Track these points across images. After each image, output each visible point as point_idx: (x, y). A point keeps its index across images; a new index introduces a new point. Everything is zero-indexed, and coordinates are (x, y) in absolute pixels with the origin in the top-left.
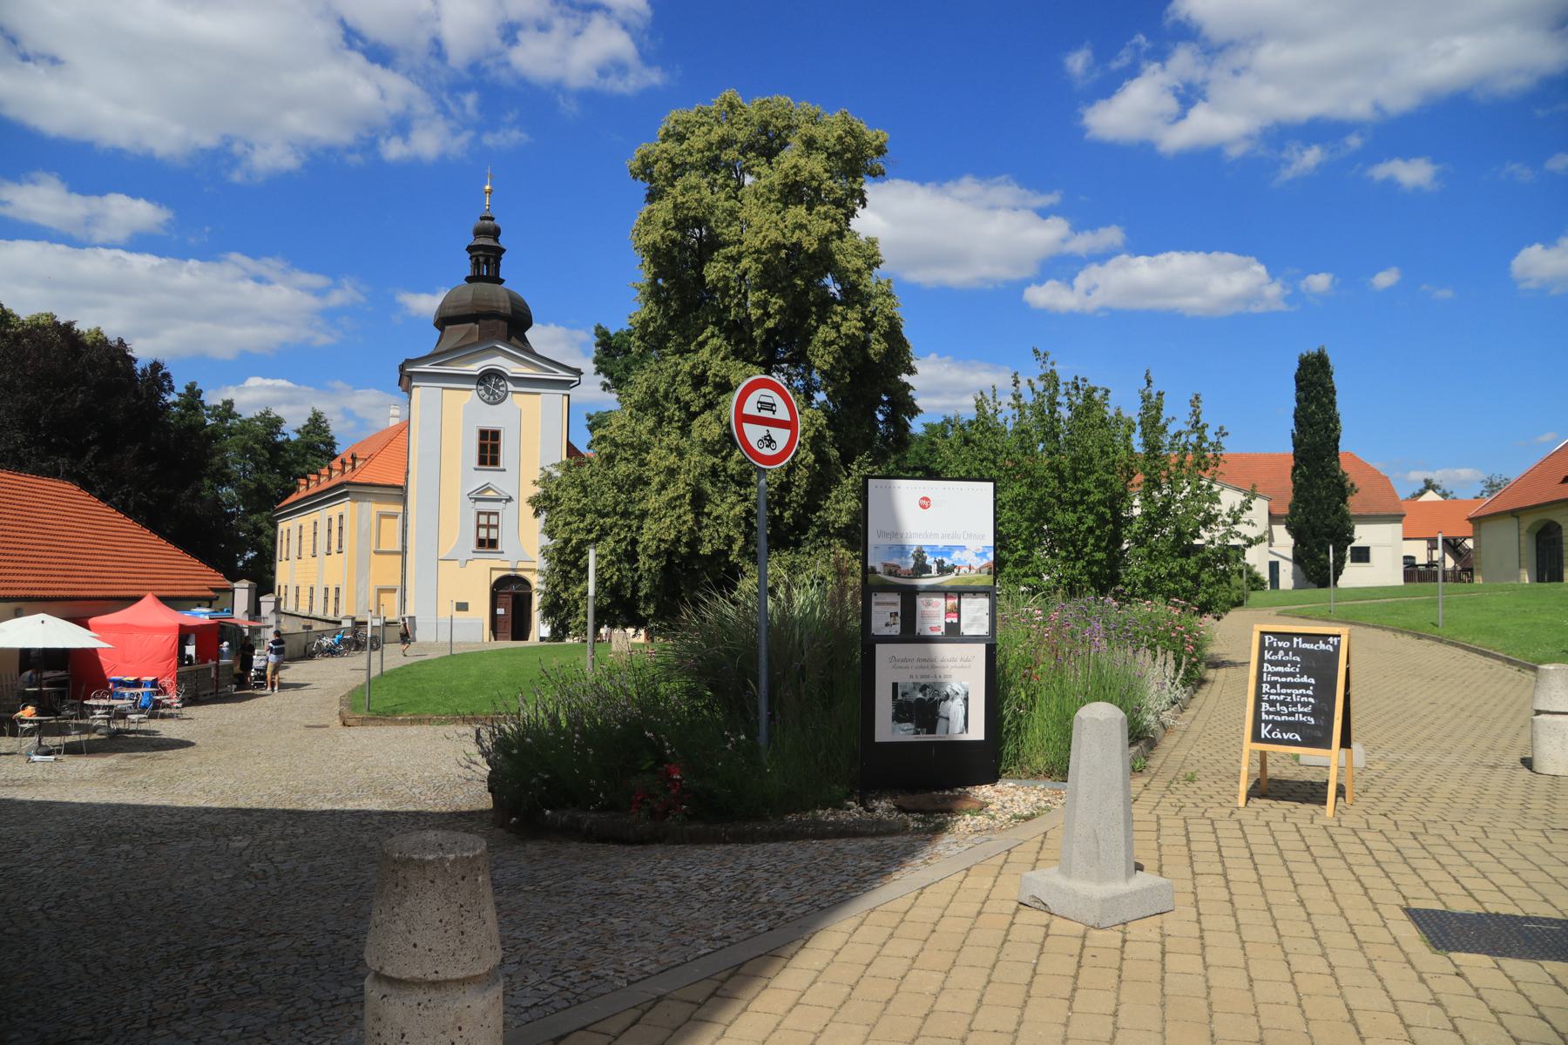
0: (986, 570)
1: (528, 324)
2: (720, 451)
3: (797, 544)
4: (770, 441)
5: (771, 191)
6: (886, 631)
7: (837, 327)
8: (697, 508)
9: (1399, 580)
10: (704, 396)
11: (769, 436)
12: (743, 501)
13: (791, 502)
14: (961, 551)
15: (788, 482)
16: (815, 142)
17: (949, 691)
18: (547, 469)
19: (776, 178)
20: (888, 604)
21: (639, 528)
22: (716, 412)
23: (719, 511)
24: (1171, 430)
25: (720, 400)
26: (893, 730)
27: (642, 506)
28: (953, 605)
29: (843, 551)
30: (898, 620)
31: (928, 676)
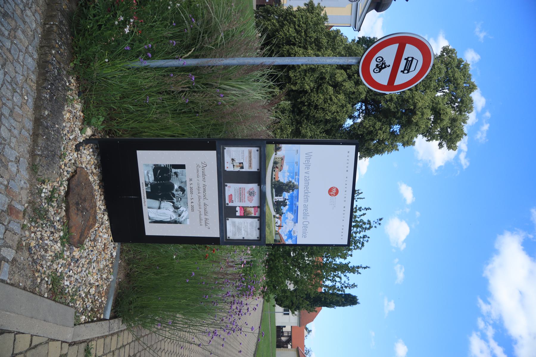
0: (278, 238)
1: (378, 10)
2: (331, 81)
3: (293, 112)
4: (381, 67)
5: (436, 104)
6: (227, 159)
7: (381, 129)
8: (308, 70)
9: (277, 324)
10: (353, 75)
11: (385, 67)
12: (311, 90)
13: (310, 109)
14: (293, 220)
15: (318, 109)
16: (454, 122)
17: (181, 209)
18: (325, 9)
19: (441, 106)
20: (250, 161)
21: (300, 47)
22: (347, 79)
23: (307, 79)
24: (342, 276)
25: (352, 82)
26: (147, 165)
27: (309, 48)
28: (250, 213)
29: (290, 130)
30: (237, 169)
31: (192, 193)
